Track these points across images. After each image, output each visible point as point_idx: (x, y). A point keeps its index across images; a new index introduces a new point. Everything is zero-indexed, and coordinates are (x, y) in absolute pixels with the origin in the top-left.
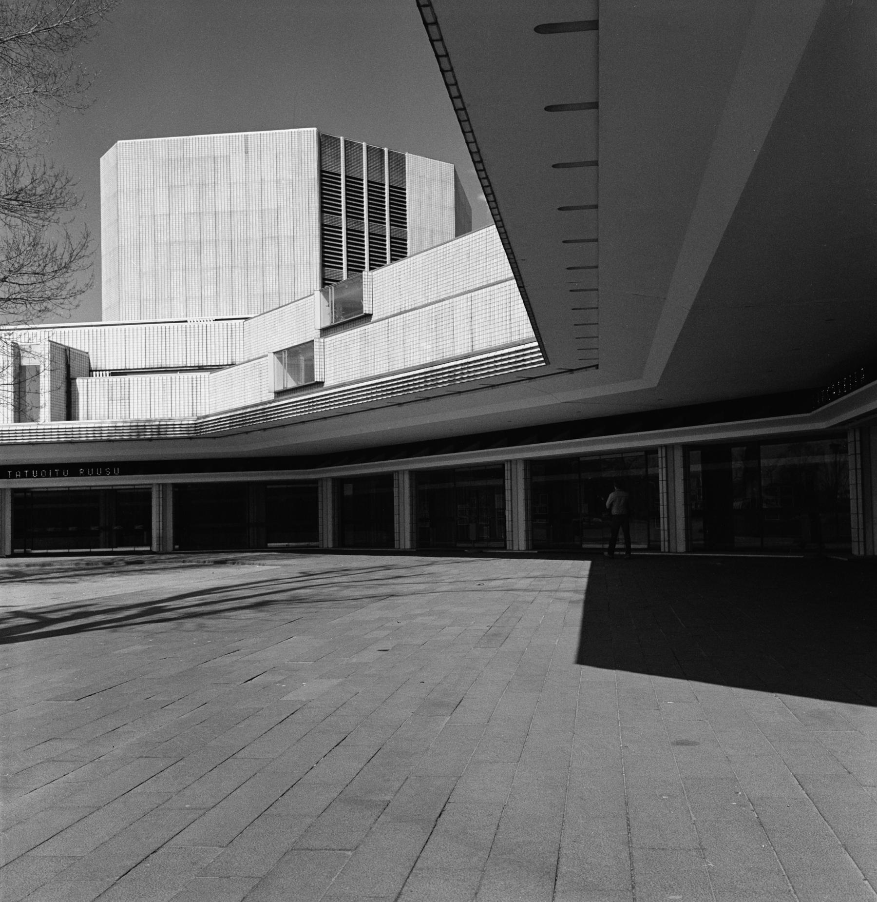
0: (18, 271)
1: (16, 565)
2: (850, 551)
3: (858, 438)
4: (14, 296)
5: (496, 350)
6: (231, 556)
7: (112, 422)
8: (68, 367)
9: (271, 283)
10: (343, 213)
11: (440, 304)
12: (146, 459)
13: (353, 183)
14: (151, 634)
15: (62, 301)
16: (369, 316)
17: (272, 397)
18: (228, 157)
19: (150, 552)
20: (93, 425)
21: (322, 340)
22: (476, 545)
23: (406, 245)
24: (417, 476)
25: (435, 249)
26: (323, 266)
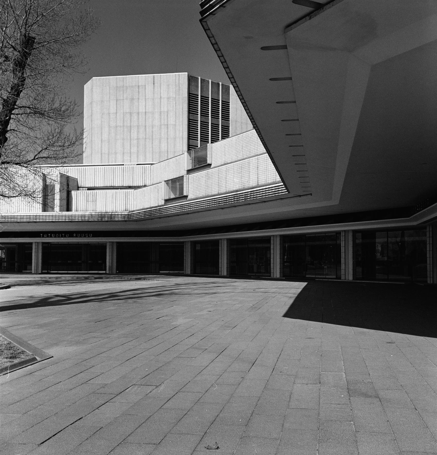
0: (53, 145)
1: (45, 278)
2: (427, 281)
3: (431, 230)
4: (50, 156)
6: (143, 276)
7: (90, 213)
8: (68, 185)
9: (164, 146)
11: (243, 161)
13: (204, 99)
14: (116, 304)
15: (72, 159)
16: (210, 165)
17: (163, 202)
19: (106, 274)
21: (187, 176)
22: (257, 275)
24: (231, 241)
25: (242, 134)
26: (189, 139)
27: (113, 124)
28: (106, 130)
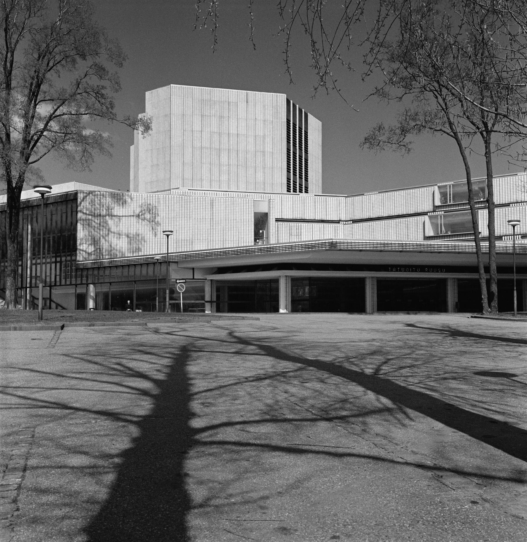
9: (260, 176)
18: (237, 103)
20: (126, 245)
27: (197, 144)
28: (188, 150)
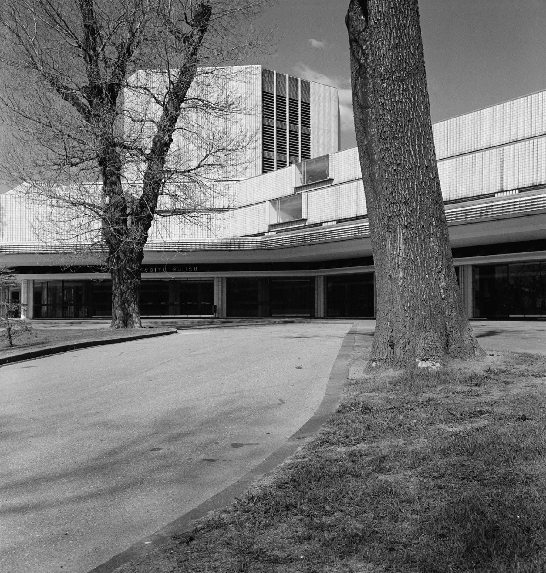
5: (509, 199)
7: (211, 240)
10: (275, 117)
12: (235, 262)
13: (281, 99)
23: (310, 138)
24: (328, 279)
